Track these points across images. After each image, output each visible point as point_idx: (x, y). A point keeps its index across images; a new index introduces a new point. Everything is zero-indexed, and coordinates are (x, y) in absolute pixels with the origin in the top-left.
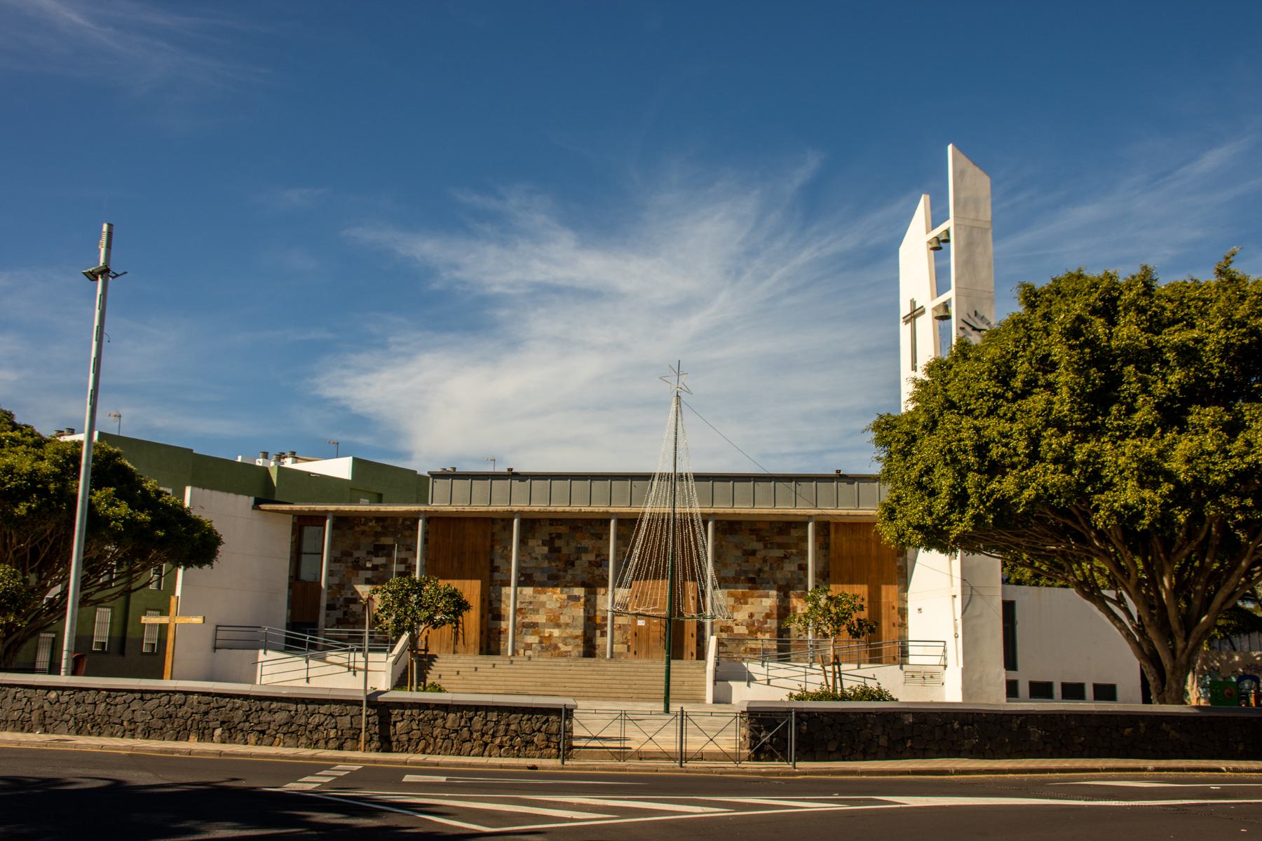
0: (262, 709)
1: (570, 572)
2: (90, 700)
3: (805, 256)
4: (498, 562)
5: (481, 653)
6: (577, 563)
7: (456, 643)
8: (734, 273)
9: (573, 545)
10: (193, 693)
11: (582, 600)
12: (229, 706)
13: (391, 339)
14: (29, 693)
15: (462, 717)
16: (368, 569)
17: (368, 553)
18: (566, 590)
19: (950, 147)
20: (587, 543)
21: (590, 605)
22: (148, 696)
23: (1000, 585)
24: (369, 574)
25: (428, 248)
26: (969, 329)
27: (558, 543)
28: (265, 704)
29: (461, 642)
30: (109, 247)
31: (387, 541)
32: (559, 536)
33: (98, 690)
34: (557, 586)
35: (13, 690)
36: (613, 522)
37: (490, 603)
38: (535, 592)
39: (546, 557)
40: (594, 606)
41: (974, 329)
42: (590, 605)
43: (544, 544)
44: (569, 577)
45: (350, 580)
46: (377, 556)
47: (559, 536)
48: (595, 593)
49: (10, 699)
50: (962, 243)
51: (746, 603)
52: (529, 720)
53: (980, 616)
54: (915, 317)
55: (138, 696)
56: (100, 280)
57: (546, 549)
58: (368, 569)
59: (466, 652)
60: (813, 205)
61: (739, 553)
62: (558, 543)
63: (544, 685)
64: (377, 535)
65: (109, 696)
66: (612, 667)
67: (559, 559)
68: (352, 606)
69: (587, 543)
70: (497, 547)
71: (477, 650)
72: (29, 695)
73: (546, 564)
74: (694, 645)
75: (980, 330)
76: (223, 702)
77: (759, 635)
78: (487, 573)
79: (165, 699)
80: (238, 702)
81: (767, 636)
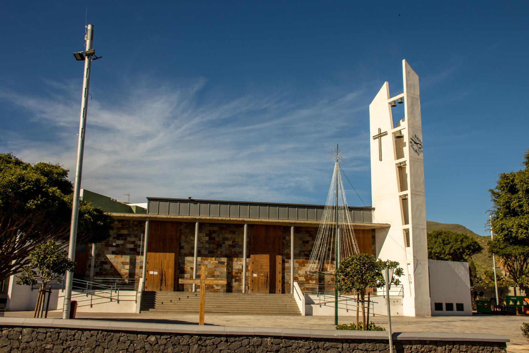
0: (318, 347)
1: (219, 250)
2: (185, 342)
3: (196, 121)
4: (183, 244)
5: (174, 290)
6: (223, 245)
7: (161, 285)
8: (167, 125)
9: (221, 236)
10: (267, 337)
11: (226, 264)
12: (294, 346)
13: (9, 142)
14: (132, 337)
15: (446, 349)
16: (113, 246)
17: (114, 238)
18: (218, 259)
19: (404, 61)
20: (228, 235)
21: (230, 266)
22: (232, 339)
23: (427, 259)
24: (114, 249)
25: (31, 103)
26: (413, 142)
27: (214, 235)
28: (321, 344)
29: (164, 285)
30: (92, 39)
31: (125, 232)
32: (214, 232)
33: (191, 335)
34: (213, 257)
35: (118, 335)
36: (245, 226)
37: (179, 265)
38: (201, 259)
39: (207, 242)
40: (232, 267)
41: (415, 143)
42: (230, 266)
43: (206, 236)
44: (219, 252)
45: (103, 252)
46: (119, 239)
47: (214, 232)
48: (232, 261)
49: (115, 342)
50: (410, 104)
51: (304, 266)
52: (483, 350)
53: (420, 273)
54: (381, 136)
55: (223, 339)
56: (87, 59)
57: (207, 238)
58: (113, 246)
59: (167, 290)
60: (201, 100)
61: (301, 242)
62: (214, 235)
63: (218, 307)
64: (119, 229)
65: (200, 339)
66: (247, 297)
67: (214, 243)
68: (104, 266)
69: (228, 235)
70: (183, 236)
71: (173, 289)
72: (132, 339)
73: (207, 246)
74: (280, 286)
75: (417, 144)
76: (290, 342)
77: (310, 281)
78: (178, 250)
79: (245, 341)
80: (302, 343)
81: (314, 282)
